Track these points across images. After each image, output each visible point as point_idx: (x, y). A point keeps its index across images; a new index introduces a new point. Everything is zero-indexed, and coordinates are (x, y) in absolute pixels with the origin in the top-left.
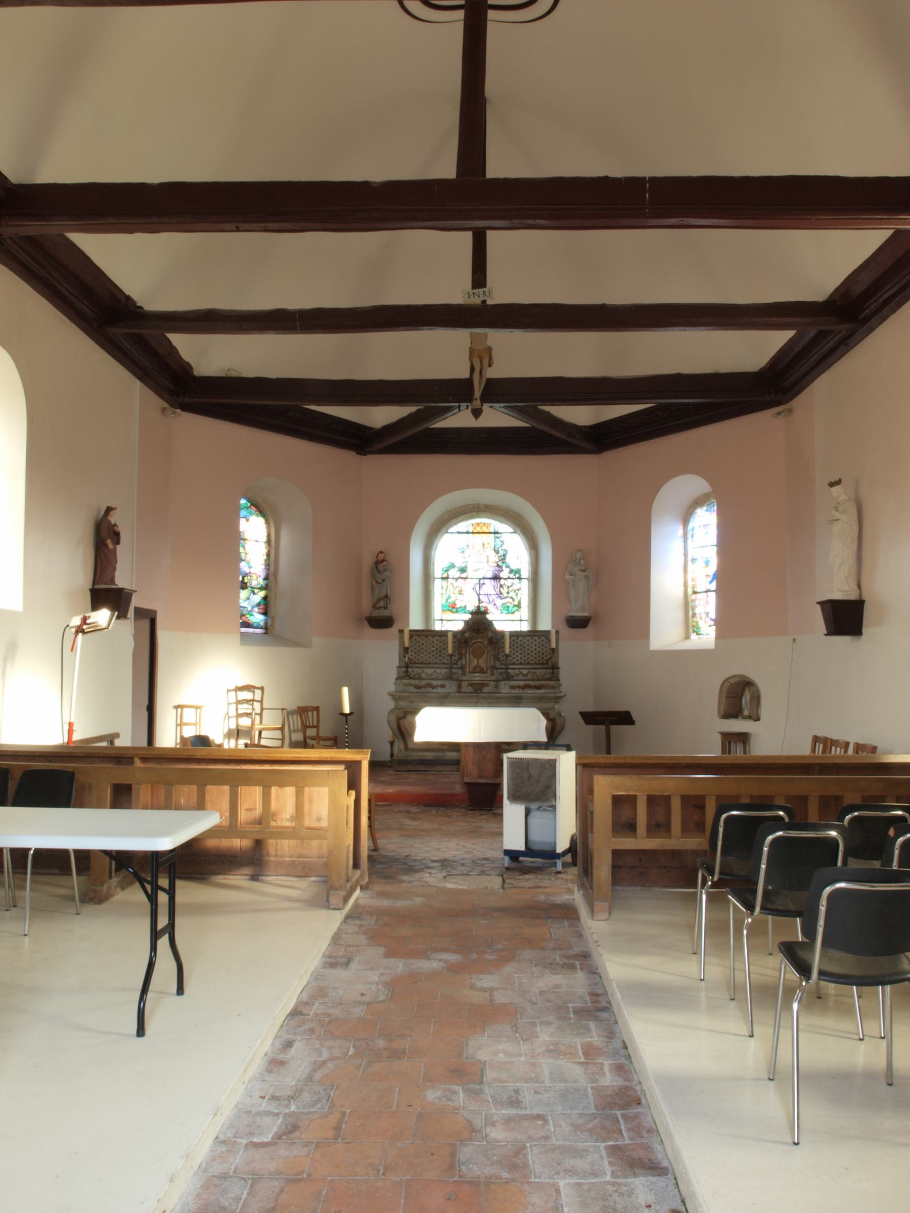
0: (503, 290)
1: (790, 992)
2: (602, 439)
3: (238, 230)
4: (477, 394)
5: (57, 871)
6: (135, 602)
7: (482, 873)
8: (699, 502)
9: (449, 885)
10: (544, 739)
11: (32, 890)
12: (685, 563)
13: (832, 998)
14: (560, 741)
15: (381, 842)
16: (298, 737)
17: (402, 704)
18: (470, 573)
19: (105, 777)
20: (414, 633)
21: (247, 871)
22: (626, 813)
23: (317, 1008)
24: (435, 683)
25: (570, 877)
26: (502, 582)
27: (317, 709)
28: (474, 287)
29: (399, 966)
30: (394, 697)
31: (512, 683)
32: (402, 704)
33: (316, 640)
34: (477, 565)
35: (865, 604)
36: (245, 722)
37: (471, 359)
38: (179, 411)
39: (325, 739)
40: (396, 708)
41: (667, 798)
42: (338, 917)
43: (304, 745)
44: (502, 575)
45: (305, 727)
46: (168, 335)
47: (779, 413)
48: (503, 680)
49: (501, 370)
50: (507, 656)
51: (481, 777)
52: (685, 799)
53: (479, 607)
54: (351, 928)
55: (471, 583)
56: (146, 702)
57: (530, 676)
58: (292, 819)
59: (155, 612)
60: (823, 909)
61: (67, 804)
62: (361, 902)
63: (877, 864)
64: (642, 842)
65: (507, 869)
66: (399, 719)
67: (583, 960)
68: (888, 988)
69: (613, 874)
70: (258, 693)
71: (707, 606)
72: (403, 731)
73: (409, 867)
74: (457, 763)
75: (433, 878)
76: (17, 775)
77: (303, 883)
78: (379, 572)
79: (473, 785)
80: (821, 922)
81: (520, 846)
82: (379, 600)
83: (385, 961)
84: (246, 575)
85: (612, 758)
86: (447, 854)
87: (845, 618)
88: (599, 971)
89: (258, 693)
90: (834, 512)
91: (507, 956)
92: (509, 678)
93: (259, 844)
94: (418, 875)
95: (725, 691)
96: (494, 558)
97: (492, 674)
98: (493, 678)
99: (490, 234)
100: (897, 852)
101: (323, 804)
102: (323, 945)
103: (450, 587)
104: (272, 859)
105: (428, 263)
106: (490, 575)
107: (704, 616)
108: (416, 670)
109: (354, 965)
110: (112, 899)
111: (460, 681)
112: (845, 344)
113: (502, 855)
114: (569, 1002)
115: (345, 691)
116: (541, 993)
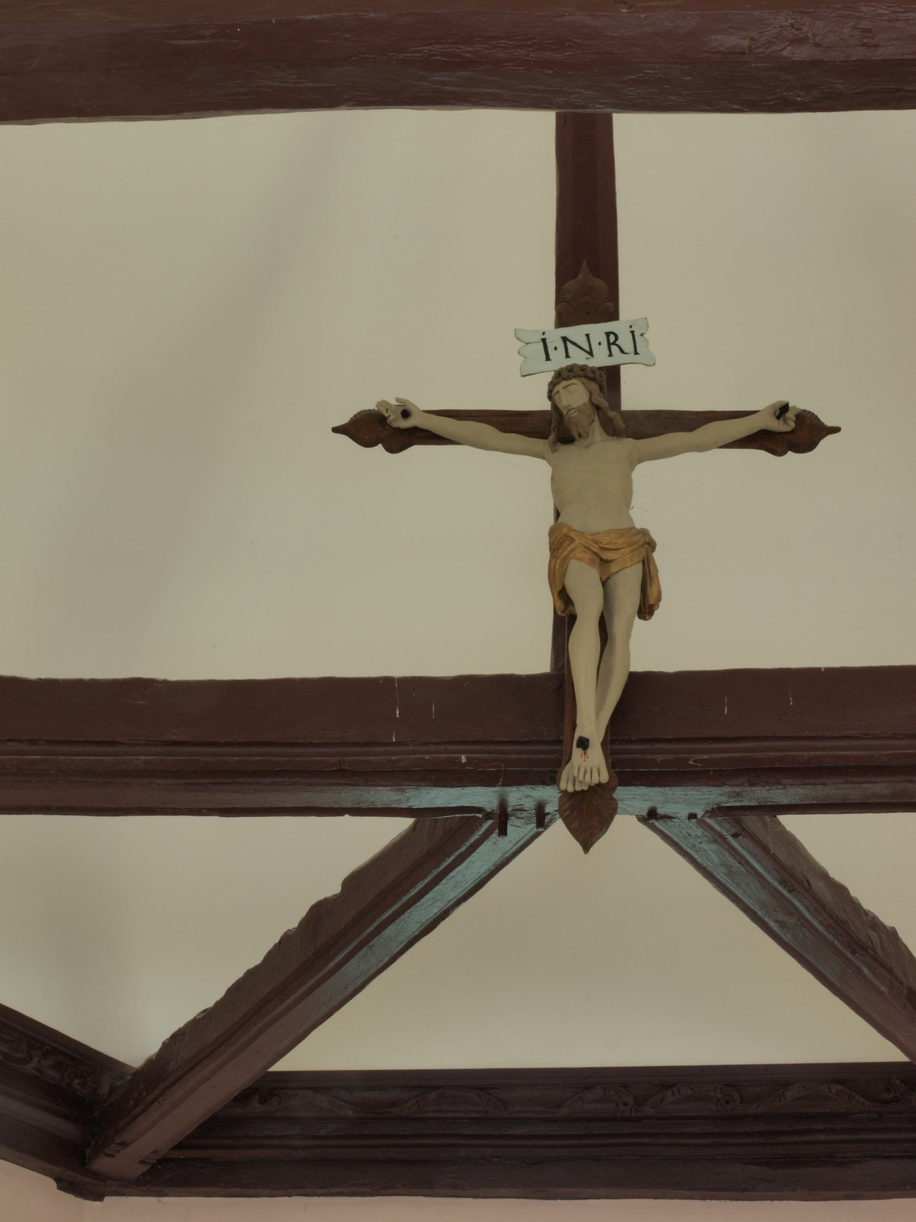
28: (562, 320)
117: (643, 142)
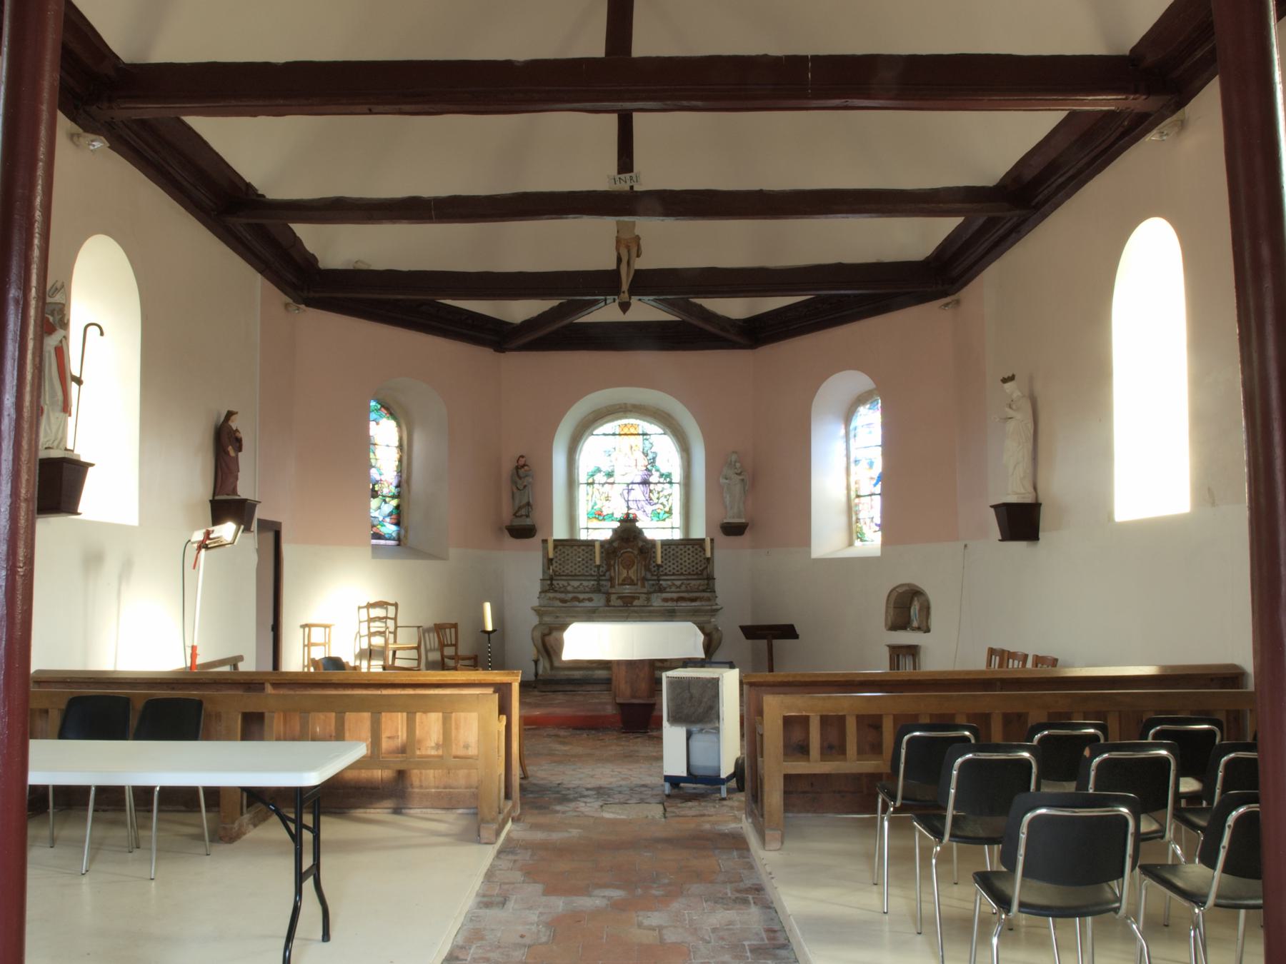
0: (653, 173)
1: (986, 924)
2: (756, 333)
3: (371, 112)
4: (625, 286)
5: (183, 808)
6: (259, 514)
7: (642, 801)
8: (861, 400)
9: (607, 815)
10: (701, 655)
11: (158, 829)
12: (847, 465)
13: (1023, 930)
14: (716, 658)
15: (530, 769)
16: (435, 656)
17: (547, 619)
18: (617, 477)
19: (233, 706)
20: (558, 543)
21: (389, 803)
22: (797, 735)
23: (473, 951)
24: (581, 596)
25: (736, 804)
26: (652, 487)
27: (455, 626)
28: (619, 173)
29: (559, 904)
30: (539, 612)
31: (665, 595)
32: (547, 619)
33: (453, 552)
34: (626, 469)
35: (1043, 509)
36: (378, 641)
37: (617, 249)
38: (303, 306)
39: (464, 659)
40: (540, 624)
41: (842, 719)
42: (490, 852)
43: (442, 665)
44: (651, 479)
45: (442, 646)
46: (292, 225)
47: (946, 305)
48: (655, 592)
49: (650, 260)
50: (659, 566)
51: (633, 697)
52: (860, 719)
53: (628, 514)
54: (505, 863)
55: (618, 489)
56: (271, 622)
57: (683, 588)
58: (438, 746)
59: (280, 524)
60: (1023, 837)
61: (194, 737)
62: (515, 835)
63: (1070, 787)
64: (815, 765)
65: (668, 796)
66: (544, 636)
67: (756, 894)
68: (1089, 919)
69: (785, 799)
70: (391, 610)
71: (871, 510)
72: (548, 647)
73: (563, 796)
74: (608, 682)
75: (589, 808)
76: (139, 705)
77: (451, 816)
78: (520, 478)
79: (628, 707)
80: (1022, 851)
81: (681, 771)
82: (520, 508)
83: (544, 899)
84: (377, 482)
85: (779, 675)
86: (599, 778)
87: (1021, 522)
88: (775, 905)
89: (391, 610)
90: (1007, 409)
91: (675, 891)
92: (662, 590)
93: (401, 775)
94: (573, 805)
95: (892, 600)
96: (643, 462)
97: (643, 586)
98: (645, 590)
99: (637, 117)
100: (1093, 774)
101: (473, 728)
102: (476, 883)
103: (596, 493)
104: (416, 790)
105: (571, 147)
106: (638, 479)
107: (868, 521)
108: (561, 583)
109: (511, 905)
110: (244, 837)
111: (608, 594)
112: (1015, 233)
113: (662, 781)
114: (746, 939)
115: (487, 607)
116: (714, 930)
117: (641, 121)
